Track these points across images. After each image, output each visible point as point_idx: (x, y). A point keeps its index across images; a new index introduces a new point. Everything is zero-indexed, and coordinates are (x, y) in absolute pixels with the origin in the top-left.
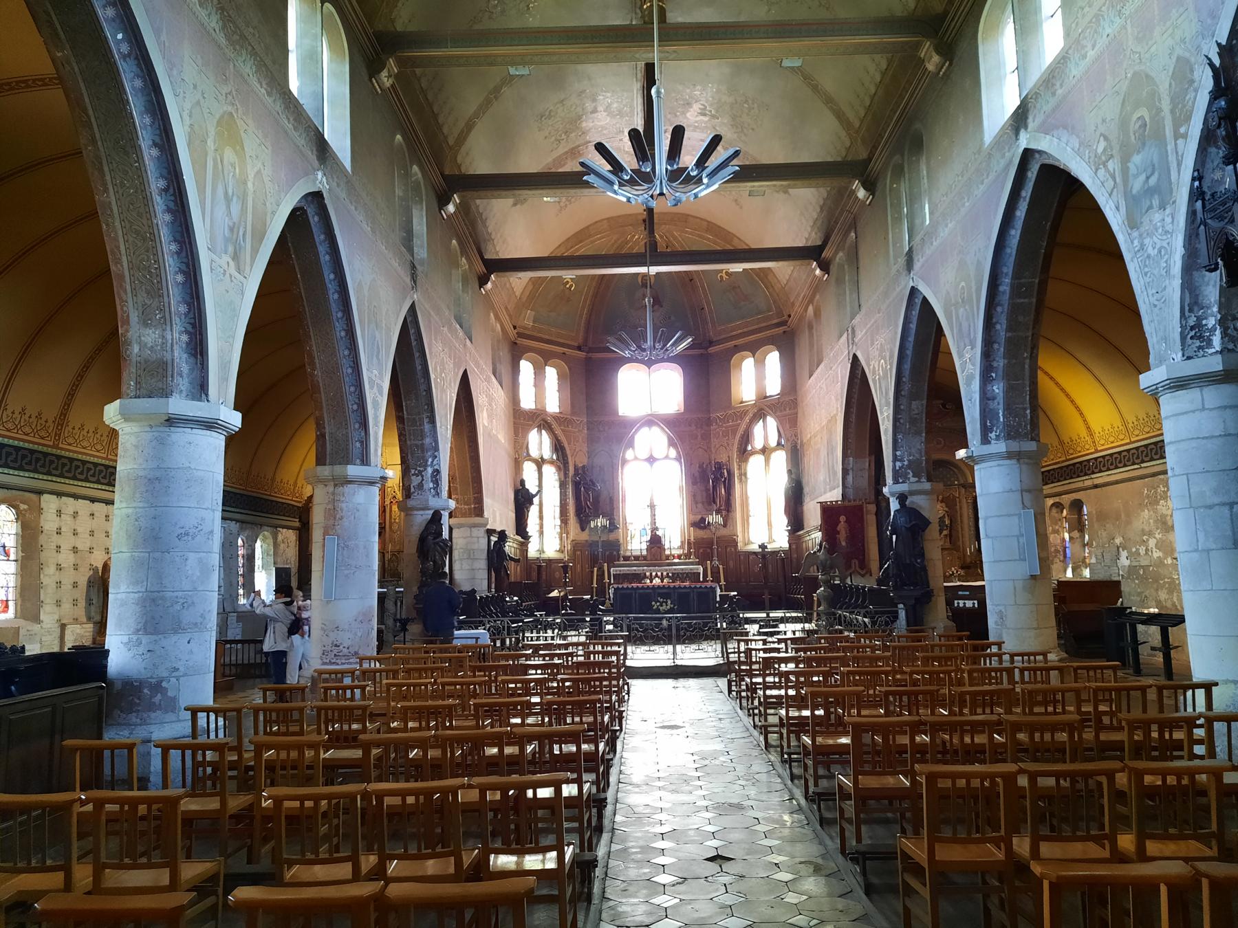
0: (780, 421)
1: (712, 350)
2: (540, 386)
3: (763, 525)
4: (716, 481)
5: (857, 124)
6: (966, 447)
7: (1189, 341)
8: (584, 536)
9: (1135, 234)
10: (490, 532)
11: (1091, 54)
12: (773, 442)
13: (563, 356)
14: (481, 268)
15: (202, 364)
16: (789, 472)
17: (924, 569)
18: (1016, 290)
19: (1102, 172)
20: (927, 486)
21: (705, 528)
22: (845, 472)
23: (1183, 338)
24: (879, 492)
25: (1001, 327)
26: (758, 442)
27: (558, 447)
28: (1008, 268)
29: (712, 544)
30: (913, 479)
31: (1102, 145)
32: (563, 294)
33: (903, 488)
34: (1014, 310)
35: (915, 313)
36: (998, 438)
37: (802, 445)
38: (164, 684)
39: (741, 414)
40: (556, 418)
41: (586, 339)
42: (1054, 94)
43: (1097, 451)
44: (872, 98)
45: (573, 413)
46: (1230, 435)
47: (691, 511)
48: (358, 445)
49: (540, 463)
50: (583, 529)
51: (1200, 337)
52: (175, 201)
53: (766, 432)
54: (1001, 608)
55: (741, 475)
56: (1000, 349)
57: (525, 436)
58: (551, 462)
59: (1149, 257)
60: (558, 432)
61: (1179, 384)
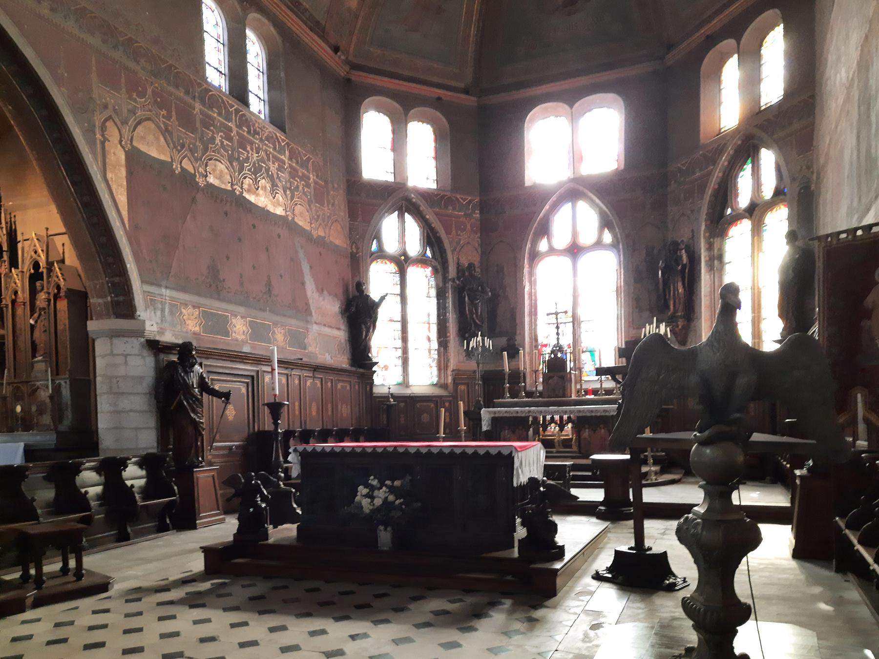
2: (399, 149)
10: (154, 346)
13: (438, 104)
26: (743, 200)
27: (431, 238)
40: (427, 196)
45: (455, 188)
49: (402, 263)
58: (422, 261)
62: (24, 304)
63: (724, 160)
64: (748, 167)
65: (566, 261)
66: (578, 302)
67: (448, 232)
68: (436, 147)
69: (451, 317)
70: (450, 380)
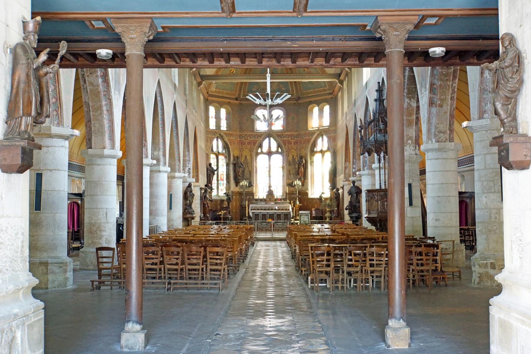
0: (329, 138)
1: (300, 101)
3: (319, 187)
4: (299, 164)
8: (237, 189)
12: (325, 148)
14: (199, 80)
16: (332, 162)
17: (359, 207)
21: (293, 186)
26: (318, 148)
27: (226, 146)
29: (298, 196)
39: (313, 133)
47: (288, 178)
49: (217, 155)
50: (237, 186)
53: (323, 143)
55: (311, 162)
58: (223, 154)
60: (226, 139)
63: (315, 136)
64: (321, 138)
65: (267, 157)
66: (269, 176)
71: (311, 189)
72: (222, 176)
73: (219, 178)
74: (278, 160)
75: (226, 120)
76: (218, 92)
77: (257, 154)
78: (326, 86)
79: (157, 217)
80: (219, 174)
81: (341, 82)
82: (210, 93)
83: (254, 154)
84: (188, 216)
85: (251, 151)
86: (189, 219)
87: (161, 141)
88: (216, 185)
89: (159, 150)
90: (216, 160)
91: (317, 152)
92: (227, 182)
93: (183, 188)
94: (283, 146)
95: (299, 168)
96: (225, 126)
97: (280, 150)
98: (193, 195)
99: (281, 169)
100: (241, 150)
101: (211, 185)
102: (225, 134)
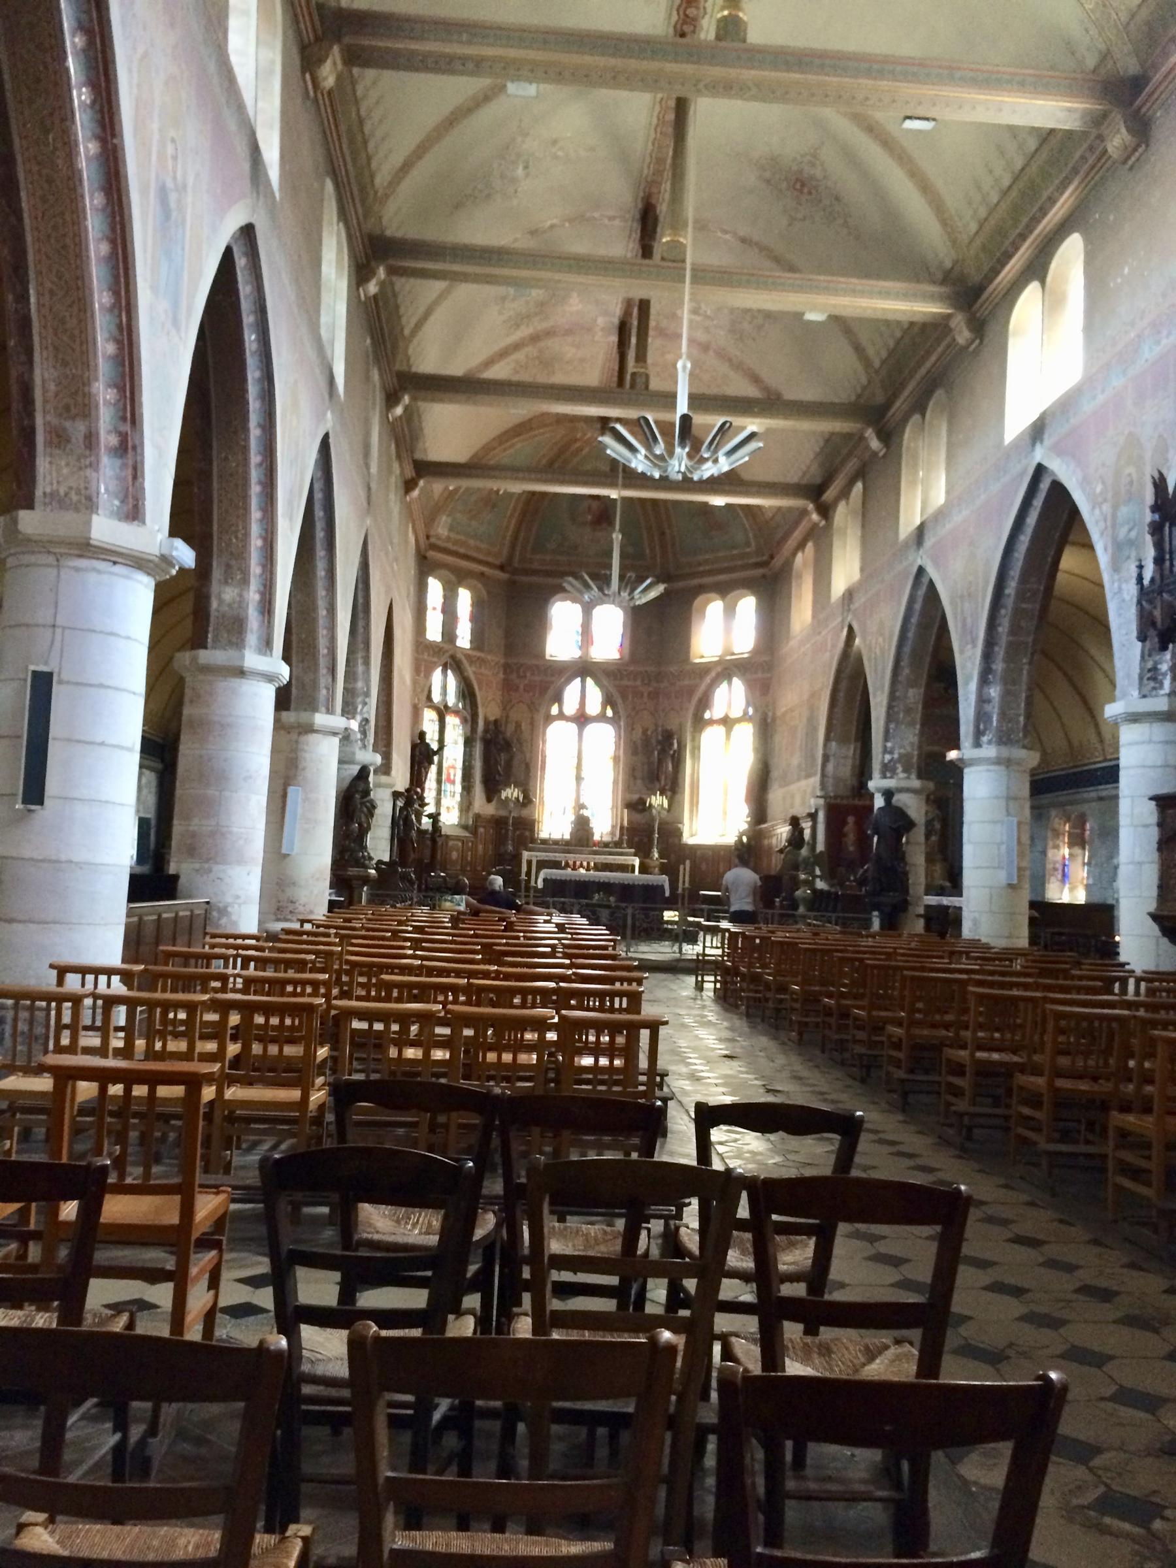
0: (750, 685)
5: (877, 364)
6: (958, 747)
7: (1145, 681)
8: (489, 810)
9: (1116, 577)
11: (1101, 398)
14: (410, 472)
15: (269, 622)
16: (756, 750)
18: (1021, 595)
19: (1097, 512)
20: (916, 783)
22: (826, 758)
23: (1141, 678)
24: (862, 786)
25: (1003, 629)
26: (716, 710)
27: (467, 693)
28: (1015, 572)
29: (646, 831)
30: (902, 775)
31: (1099, 489)
32: (492, 501)
33: (889, 783)
34: (1018, 613)
35: (921, 592)
36: (990, 742)
37: (774, 719)
38: (229, 909)
41: (511, 557)
42: (1067, 421)
43: (1105, 760)
44: (898, 343)
46: (1168, 766)
47: (628, 788)
48: (324, 692)
49: (442, 712)
50: (489, 800)
51: (1154, 679)
52: (266, 475)
53: (730, 698)
54: (976, 915)
56: (1000, 652)
57: (428, 675)
58: (456, 712)
59: (1123, 601)
60: (470, 671)
61: (1135, 718)
62: (683, 898)
63: (708, 680)
64: (725, 685)
65: (573, 727)
66: (577, 780)
67: (480, 689)
68: (472, 612)
69: (478, 765)
70: (471, 822)
71: (691, 819)
72: (452, 772)
73: (444, 777)
74: (604, 741)
75: (471, 620)
76: (456, 542)
77: (549, 719)
78: (748, 544)
79: (216, 868)
80: (445, 765)
81: (826, 511)
82: (433, 540)
83: (540, 717)
84: (353, 871)
85: (533, 708)
86: (355, 883)
87: (256, 542)
88: (433, 793)
89: (245, 581)
90: (437, 727)
91: (711, 722)
92: (463, 788)
93: (340, 780)
94: (619, 701)
95: (660, 761)
96: (468, 637)
97: (609, 712)
98: (371, 808)
99: (611, 764)
100: (506, 706)
101: (423, 790)
102: (468, 657)
